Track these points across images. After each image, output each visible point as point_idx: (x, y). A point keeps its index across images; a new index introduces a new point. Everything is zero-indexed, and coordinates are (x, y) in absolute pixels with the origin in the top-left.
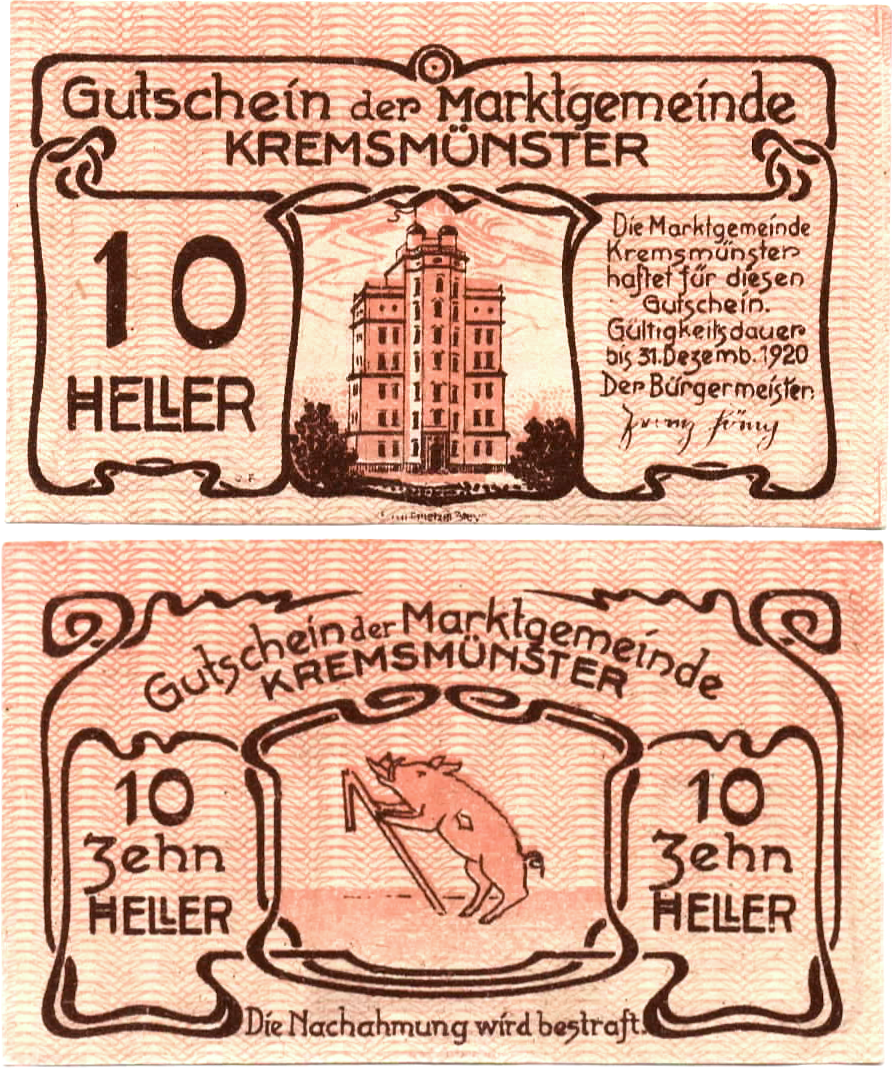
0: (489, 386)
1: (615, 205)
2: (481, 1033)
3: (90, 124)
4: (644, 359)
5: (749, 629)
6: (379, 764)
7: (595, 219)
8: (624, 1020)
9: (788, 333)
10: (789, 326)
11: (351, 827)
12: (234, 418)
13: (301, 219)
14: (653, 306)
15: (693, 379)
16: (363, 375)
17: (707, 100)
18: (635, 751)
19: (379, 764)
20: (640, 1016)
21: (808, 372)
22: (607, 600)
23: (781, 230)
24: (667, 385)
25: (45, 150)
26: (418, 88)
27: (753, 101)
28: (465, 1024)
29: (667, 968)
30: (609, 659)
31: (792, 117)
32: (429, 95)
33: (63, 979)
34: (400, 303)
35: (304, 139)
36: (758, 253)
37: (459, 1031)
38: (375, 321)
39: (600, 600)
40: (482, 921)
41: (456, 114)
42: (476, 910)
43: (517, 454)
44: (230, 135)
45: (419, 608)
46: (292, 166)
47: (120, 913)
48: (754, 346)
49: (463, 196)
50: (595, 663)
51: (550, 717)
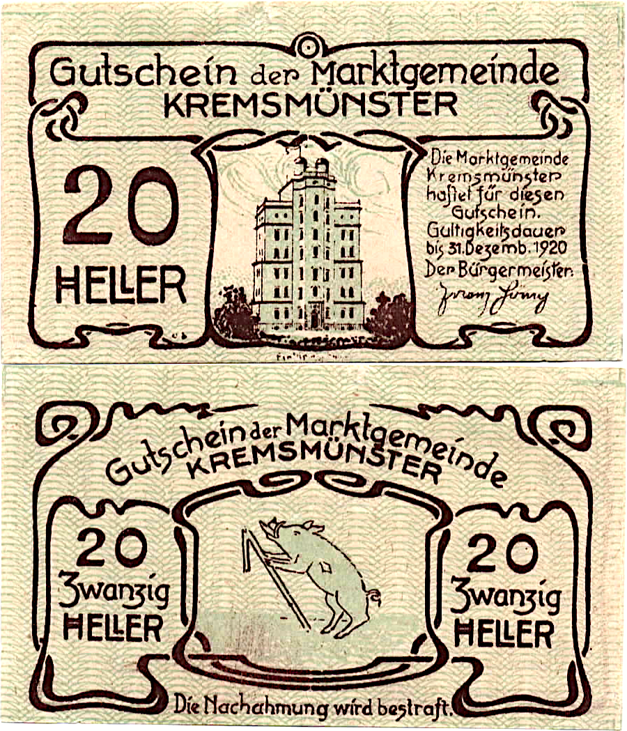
0: (351, 270)
1: (434, 143)
2: (338, 713)
3: (70, 89)
4: (452, 250)
5: (526, 430)
6: (268, 525)
7: (422, 153)
8: (438, 705)
9: (553, 233)
10: (554, 228)
11: (247, 569)
12: (172, 293)
13: (217, 154)
14: (459, 214)
15: (487, 264)
16: (264, 262)
17: (498, 69)
18: (447, 517)
19: (268, 525)
20: (449, 701)
21: (571, 258)
22: (430, 413)
23: (548, 160)
25: (39, 109)
26: (297, 63)
27: (530, 69)
28: (326, 707)
29: (468, 669)
30: (429, 457)
32: (305, 67)
33: (45, 670)
34: (288, 211)
35: (218, 99)
36: (532, 176)
37: (323, 711)
38: (273, 225)
39: (423, 412)
40: (336, 637)
41: (323, 80)
42: (333, 629)
43: (370, 317)
44: (167, 96)
45: (298, 417)
46: (233, 468)
47: (85, 623)
48: (529, 242)
49: (330, 140)
50: (419, 460)
51: (388, 494)
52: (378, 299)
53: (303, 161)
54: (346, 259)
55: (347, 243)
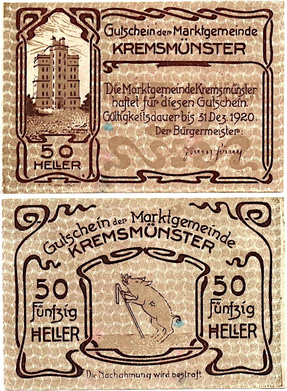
24: (181, 130)
29: (215, 353)
31: (256, 35)
33: (22, 360)
52: (86, 96)
53: (54, 38)
54: (72, 79)
55: (73, 73)
